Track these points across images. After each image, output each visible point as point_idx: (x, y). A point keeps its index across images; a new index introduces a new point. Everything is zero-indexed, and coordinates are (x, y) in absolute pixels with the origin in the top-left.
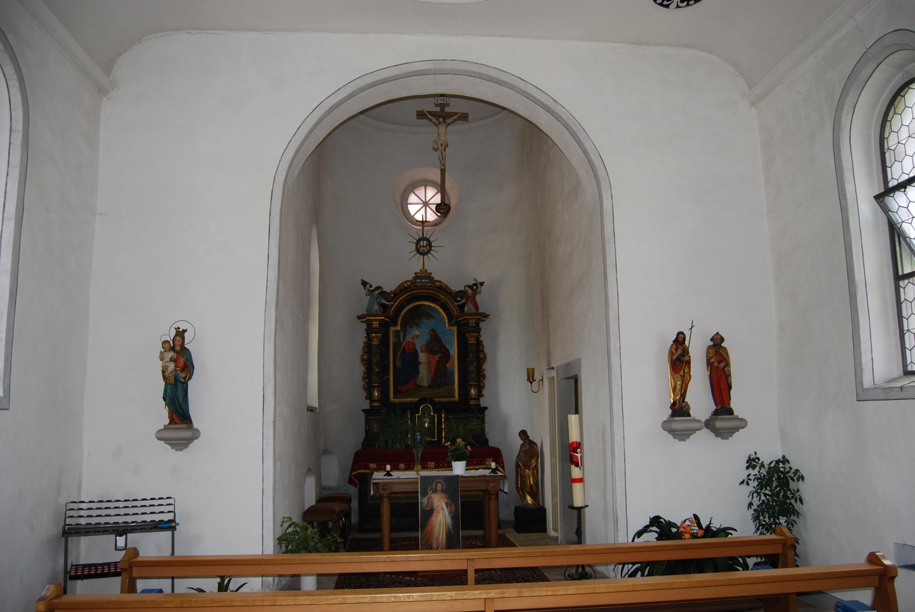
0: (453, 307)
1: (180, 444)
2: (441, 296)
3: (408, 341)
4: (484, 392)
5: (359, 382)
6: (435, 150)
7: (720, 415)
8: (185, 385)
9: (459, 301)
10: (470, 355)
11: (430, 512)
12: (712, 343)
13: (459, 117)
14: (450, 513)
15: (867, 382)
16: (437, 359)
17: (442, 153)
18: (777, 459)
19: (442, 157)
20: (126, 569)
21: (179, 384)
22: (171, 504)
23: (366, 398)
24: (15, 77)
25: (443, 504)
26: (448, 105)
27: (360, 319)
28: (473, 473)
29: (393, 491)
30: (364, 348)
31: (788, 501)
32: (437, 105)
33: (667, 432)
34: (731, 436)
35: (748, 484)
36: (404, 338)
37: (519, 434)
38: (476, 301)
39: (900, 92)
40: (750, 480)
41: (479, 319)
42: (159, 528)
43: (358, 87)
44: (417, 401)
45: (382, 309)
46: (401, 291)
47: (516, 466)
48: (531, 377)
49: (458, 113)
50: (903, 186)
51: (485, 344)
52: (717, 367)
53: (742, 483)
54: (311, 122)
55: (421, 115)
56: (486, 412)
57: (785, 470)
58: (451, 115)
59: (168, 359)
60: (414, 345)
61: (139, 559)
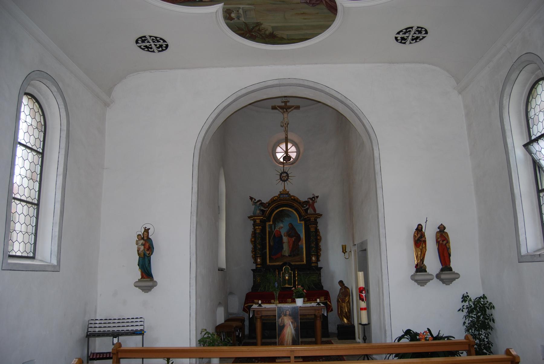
0: (301, 210)
1: (147, 289)
2: (295, 205)
3: (277, 230)
4: (321, 258)
5: (250, 254)
6: (282, 126)
7: (444, 271)
8: (149, 258)
9: (305, 207)
10: (312, 238)
11: (282, 327)
12: (438, 230)
13: (295, 108)
14: (294, 327)
15: (523, 252)
16: (293, 240)
17: (286, 128)
18: (479, 296)
19: (286, 130)
20: (115, 353)
21: (146, 257)
22: (142, 321)
23: (254, 263)
24: (62, 103)
25: (290, 323)
26: (289, 102)
27: (249, 218)
28: (308, 305)
29: (263, 315)
30: (252, 235)
31: (486, 321)
32: (282, 102)
33: (414, 281)
34: (451, 283)
35: (462, 311)
36: (275, 229)
37: (339, 283)
38: (314, 207)
39: (534, 87)
40: (464, 308)
41: (316, 217)
42: (135, 334)
43: (238, 96)
44: (281, 264)
45: (261, 212)
46: (272, 202)
47: (337, 301)
48: (344, 251)
49: (294, 106)
50: (537, 140)
51: (320, 231)
52: (442, 243)
53: (459, 310)
54: (214, 116)
55: (274, 108)
56: (321, 270)
57: (484, 303)
58: (290, 107)
59: (140, 244)
60: (280, 232)
61: (122, 348)
